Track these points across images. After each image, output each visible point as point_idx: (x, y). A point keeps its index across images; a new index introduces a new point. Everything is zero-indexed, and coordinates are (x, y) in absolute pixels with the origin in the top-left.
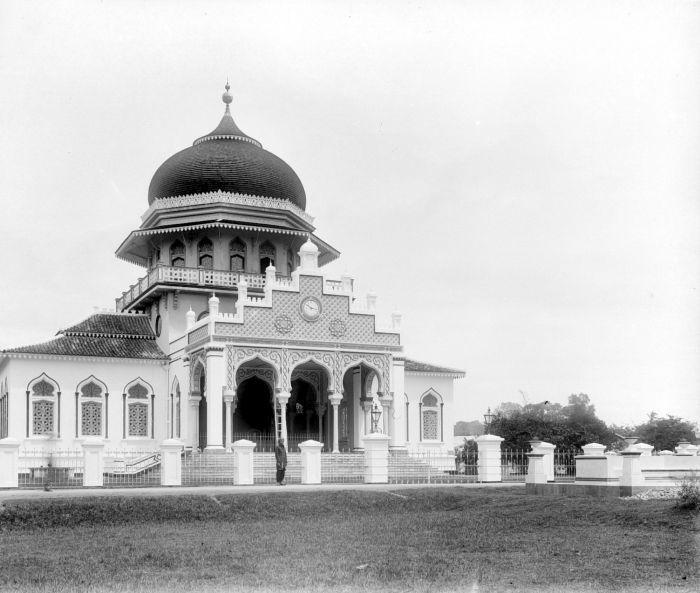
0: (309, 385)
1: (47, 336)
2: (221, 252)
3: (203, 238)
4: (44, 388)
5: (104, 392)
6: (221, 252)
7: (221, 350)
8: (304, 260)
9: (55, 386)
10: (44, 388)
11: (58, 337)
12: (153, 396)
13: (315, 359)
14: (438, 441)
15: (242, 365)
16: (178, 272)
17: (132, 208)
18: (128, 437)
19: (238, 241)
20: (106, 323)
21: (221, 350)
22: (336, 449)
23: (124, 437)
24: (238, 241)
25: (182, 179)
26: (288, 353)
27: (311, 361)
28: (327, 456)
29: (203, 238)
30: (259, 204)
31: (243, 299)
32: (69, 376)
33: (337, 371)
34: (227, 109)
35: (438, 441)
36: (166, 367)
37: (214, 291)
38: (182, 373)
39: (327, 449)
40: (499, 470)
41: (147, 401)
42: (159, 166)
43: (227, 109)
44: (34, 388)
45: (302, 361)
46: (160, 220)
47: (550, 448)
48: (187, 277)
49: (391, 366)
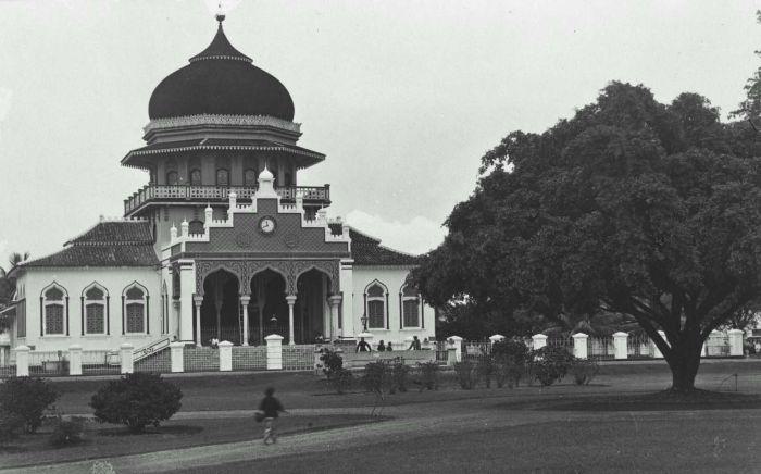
0: (269, 285)
1: (54, 246)
2: (208, 171)
3: (194, 159)
4: (54, 293)
5: (385, 292)
6: (208, 171)
7: (190, 264)
8: (261, 184)
9: (144, 290)
10: (54, 293)
11: (66, 248)
12: (108, 298)
13: (271, 268)
14: (64, 335)
15: (209, 275)
16: (196, 189)
17: (133, 127)
18: (404, 329)
19: (223, 159)
20: (104, 231)
21: (190, 264)
22: (292, 343)
23: (123, 333)
24: (223, 159)
25: (171, 97)
26: (294, 263)
27: (314, 269)
28: (286, 347)
29: (194, 159)
30: (176, 124)
31: (233, 208)
32: (75, 284)
33: (292, 275)
34: (220, 27)
35: (64, 335)
36: (159, 272)
37: (209, 204)
38: (167, 275)
39: (285, 341)
40: (280, 361)
41: (63, 302)
42: (161, 80)
43: (220, 27)
44: (47, 294)
45: (213, 270)
46: (155, 139)
47: (180, 347)
48: (159, 194)
49: (341, 271)
